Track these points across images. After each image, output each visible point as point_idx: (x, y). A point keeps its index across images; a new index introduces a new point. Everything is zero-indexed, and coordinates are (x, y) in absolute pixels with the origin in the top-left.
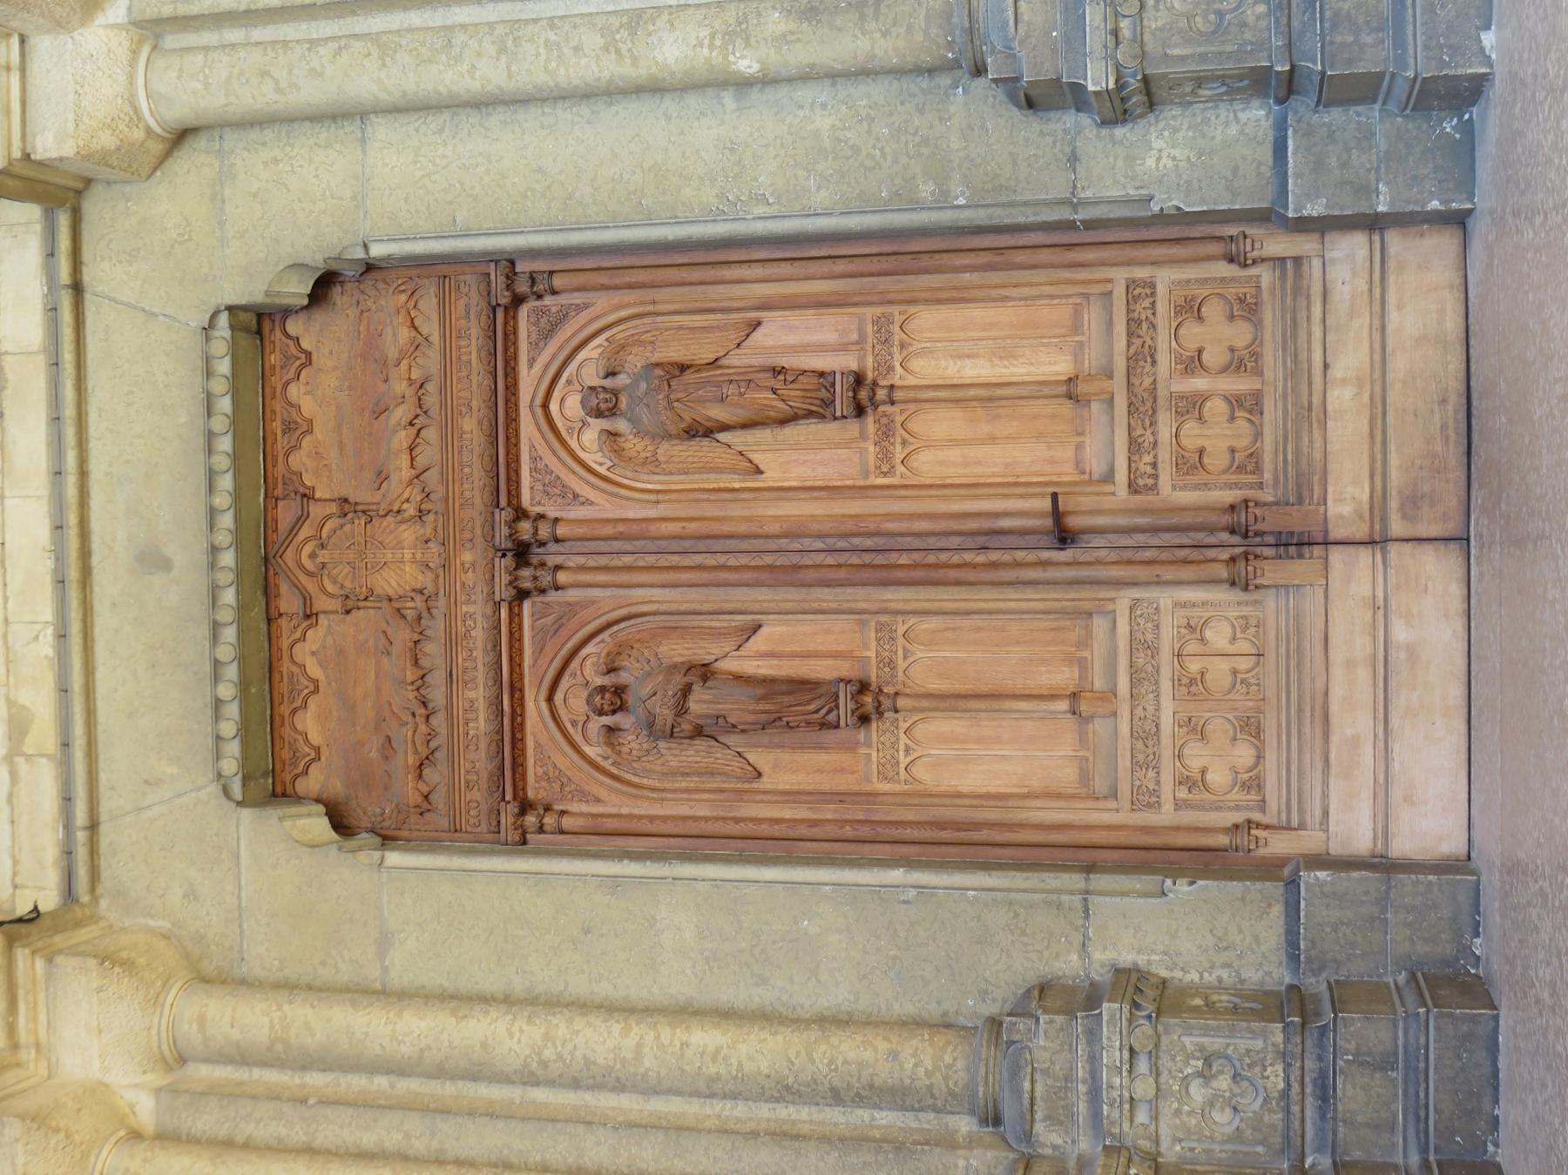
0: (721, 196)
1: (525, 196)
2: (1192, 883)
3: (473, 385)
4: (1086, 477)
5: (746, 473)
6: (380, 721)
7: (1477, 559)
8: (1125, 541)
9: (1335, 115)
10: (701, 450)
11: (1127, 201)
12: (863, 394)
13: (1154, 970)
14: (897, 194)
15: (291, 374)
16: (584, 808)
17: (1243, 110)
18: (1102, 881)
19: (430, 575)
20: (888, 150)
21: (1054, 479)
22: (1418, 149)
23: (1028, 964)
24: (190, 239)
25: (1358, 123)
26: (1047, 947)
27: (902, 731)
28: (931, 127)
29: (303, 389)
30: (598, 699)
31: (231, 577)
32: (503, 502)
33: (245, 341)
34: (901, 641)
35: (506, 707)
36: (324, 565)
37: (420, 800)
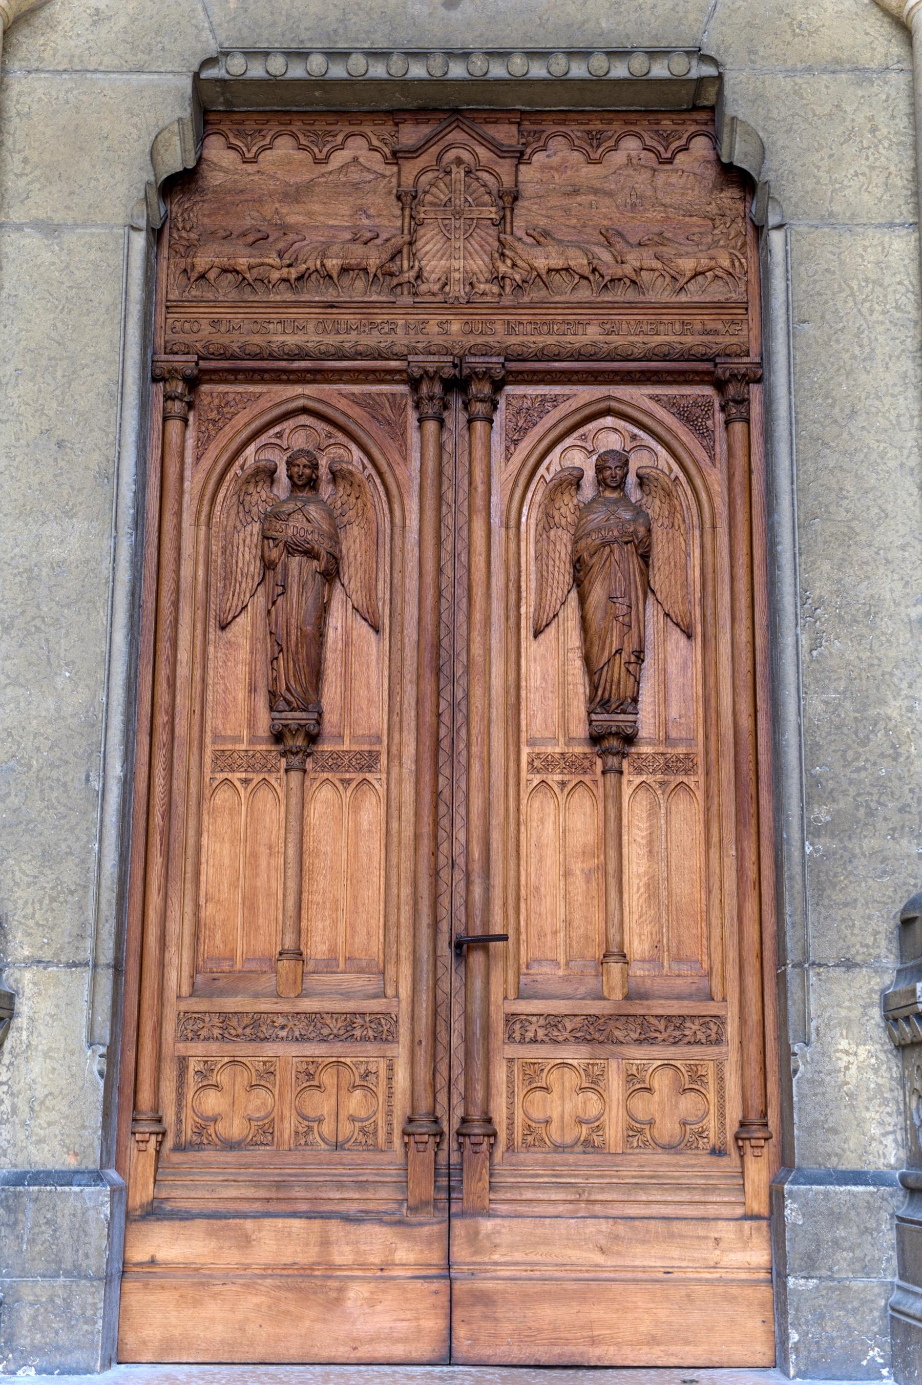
0: (821, 601)
1: (826, 397)
2: (101, 1074)
3: (633, 336)
4: (524, 970)
5: (536, 622)
6: (285, 229)
7: (429, 1373)
8: (457, 1010)
9: (889, 1237)
10: (562, 574)
11: (805, 1018)
12: (614, 743)
13: (12, 1034)
14: (818, 782)
15: (649, 142)
16: (190, 443)
17: (895, 1141)
18: (106, 980)
19: (436, 288)
20: (863, 774)
21: (523, 937)
22: (851, 1320)
23: (20, 903)
24: (795, 35)
25: (880, 1260)
26: (37, 924)
27: (266, 776)
28: (885, 819)
29: (633, 153)
30: (304, 461)
31: (438, 73)
32: (513, 366)
33: (685, 93)
34: (359, 777)
35: (297, 365)
36: (449, 173)
37: (200, 269)
